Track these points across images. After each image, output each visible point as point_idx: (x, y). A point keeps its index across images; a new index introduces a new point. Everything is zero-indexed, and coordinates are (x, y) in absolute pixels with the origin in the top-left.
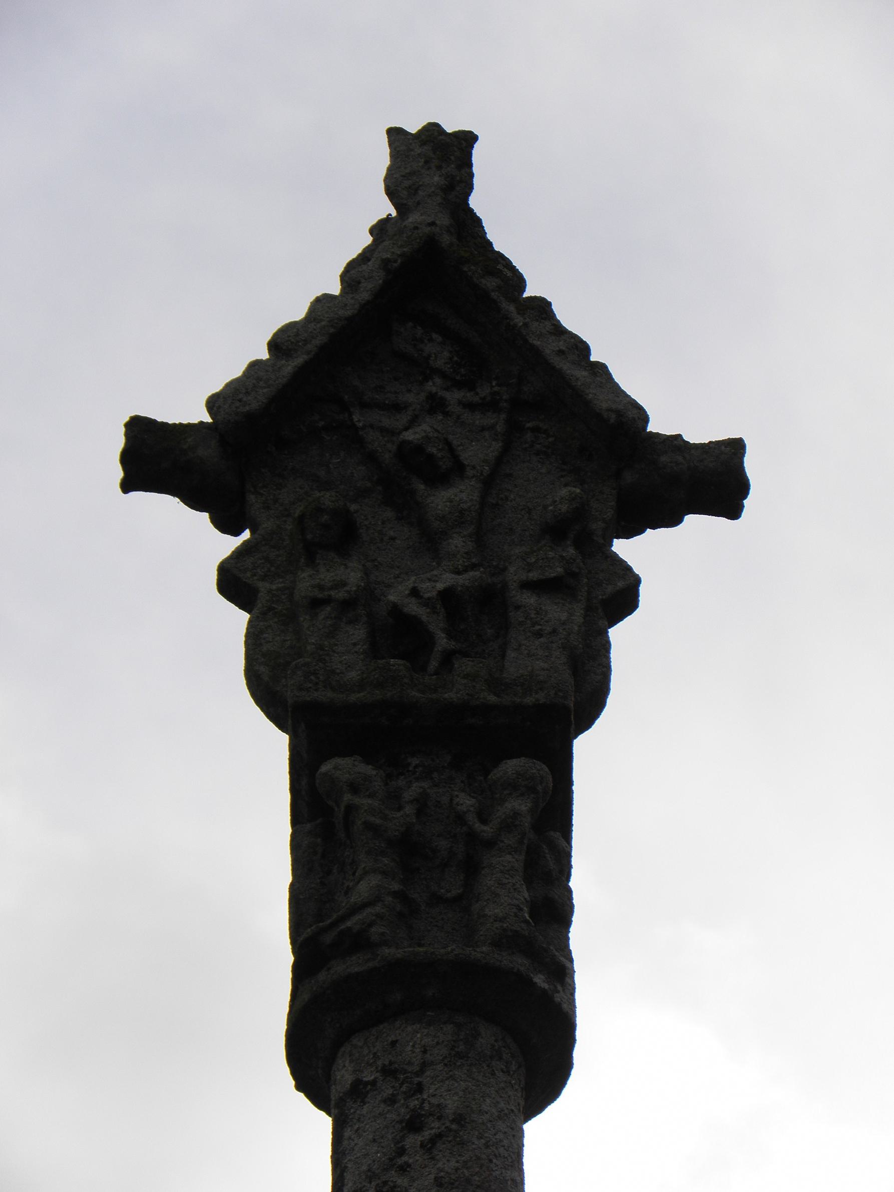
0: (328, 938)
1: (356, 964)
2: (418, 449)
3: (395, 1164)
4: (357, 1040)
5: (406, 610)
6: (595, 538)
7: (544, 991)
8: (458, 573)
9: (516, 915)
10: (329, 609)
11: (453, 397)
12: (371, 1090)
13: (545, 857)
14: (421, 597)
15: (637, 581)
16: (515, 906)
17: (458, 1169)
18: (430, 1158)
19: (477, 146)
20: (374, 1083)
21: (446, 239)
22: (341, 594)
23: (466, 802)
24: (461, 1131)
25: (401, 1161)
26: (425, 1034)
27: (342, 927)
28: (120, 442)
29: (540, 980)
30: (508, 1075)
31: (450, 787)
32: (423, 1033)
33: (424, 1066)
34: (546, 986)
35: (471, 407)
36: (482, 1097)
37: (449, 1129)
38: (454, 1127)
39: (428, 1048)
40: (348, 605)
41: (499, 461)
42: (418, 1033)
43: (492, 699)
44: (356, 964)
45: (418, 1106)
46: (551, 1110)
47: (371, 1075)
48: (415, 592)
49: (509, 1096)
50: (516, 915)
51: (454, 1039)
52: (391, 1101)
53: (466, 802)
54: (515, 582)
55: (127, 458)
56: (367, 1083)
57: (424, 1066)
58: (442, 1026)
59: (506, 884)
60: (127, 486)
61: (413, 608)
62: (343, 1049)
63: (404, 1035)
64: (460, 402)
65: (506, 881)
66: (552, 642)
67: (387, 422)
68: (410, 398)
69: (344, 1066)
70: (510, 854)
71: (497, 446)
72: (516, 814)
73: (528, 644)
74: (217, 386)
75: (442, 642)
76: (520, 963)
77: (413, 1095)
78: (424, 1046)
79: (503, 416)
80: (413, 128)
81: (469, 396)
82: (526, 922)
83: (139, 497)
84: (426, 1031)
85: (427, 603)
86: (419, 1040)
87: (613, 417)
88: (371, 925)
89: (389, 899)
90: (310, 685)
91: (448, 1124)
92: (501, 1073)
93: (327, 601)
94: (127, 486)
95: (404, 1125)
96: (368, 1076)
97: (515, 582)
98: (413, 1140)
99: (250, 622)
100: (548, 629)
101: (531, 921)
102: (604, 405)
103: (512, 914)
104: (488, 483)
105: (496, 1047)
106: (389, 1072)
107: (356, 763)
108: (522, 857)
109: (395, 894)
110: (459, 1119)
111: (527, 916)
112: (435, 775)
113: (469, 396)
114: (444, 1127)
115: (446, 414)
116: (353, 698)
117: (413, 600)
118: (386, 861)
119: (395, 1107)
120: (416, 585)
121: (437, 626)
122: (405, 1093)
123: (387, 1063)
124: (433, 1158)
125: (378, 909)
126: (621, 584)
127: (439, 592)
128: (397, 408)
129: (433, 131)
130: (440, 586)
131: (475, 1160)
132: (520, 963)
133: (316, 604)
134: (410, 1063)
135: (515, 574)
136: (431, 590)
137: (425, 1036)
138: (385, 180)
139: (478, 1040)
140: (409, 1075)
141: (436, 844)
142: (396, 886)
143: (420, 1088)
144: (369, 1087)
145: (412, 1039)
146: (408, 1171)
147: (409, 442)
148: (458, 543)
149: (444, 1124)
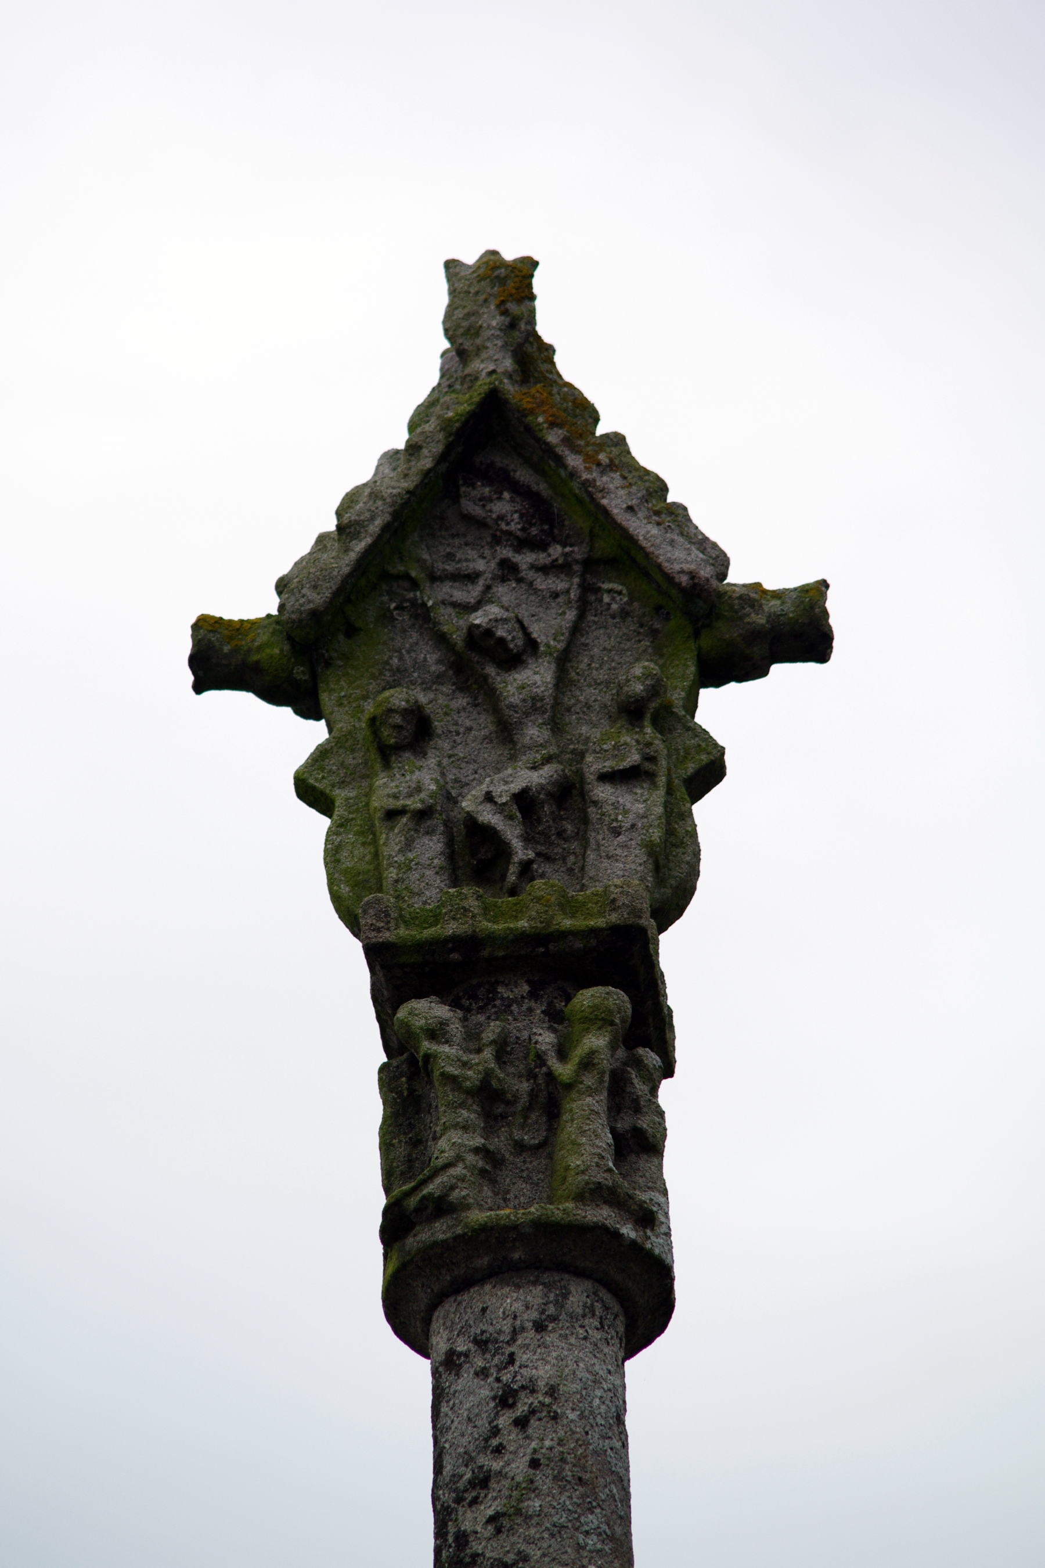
0: (413, 1202)
1: (440, 1231)
2: (488, 633)
3: (490, 1446)
4: (449, 1305)
5: (481, 819)
6: (675, 710)
7: (633, 1242)
8: (534, 768)
9: (598, 1165)
10: (405, 820)
11: (525, 559)
12: (464, 1362)
13: (632, 1083)
14: (496, 803)
15: (722, 751)
16: (598, 1155)
17: (554, 1447)
18: (524, 1438)
19: (538, 274)
20: (466, 1355)
21: (510, 388)
22: (415, 804)
23: (546, 1039)
24: (554, 1404)
25: (495, 1442)
26: (514, 1298)
27: (425, 1192)
28: (186, 646)
29: (628, 1231)
30: (603, 1331)
31: (529, 1020)
32: (512, 1297)
33: (515, 1333)
34: (633, 1235)
35: (544, 570)
36: (576, 1362)
37: (542, 1404)
38: (547, 1400)
39: (518, 1314)
40: (423, 815)
41: (576, 629)
42: (507, 1297)
43: (567, 923)
44: (440, 1231)
45: (510, 1380)
46: (660, 1343)
47: (464, 1346)
48: (489, 798)
49: (605, 1355)
50: (598, 1165)
51: (544, 1301)
52: (482, 1373)
53: (546, 1039)
54: (591, 774)
55: (196, 662)
56: (460, 1354)
57: (515, 1333)
58: (531, 1288)
59: (587, 1130)
60: (199, 688)
61: (488, 816)
62: (436, 1314)
63: (494, 1300)
64: (533, 567)
65: (587, 1128)
66: (631, 839)
67: (460, 595)
68: (480, 565)
69: (439, 1333)
70: (590, 1096)
71: (571, 615)
72: (592, 1053)
73: (606, 845)
74: (285, 568)
75: (521, 852)
76: (603, 1214)
77: (505, 1368)
78: (514, 1312)
79: (576, 580)
80: (470, 257)
81: (542, 558)
82: (610, 1170)
83: (214, 697)
84: (515, 1295)
85: (501, 808)
86: (509, 1305)
87: (684, 579)
88: (452, 1188)
89: (471, 1158)
90: (382, 924)
91: (541, 1398)
92: (596, 1331)
93: (401, 812)
94: (199, 688)
95: (497, 1401)
96: (462, 1346)
97: (591, 774)
98: (504, 1420)
99: (330, 833)
100: (626, 825)
101: (614, 1169)
102: (677, 567)
103: (594, 1164)
104: (564, 660)
105: (588, 1305)
106: (482, 1343)
107: (433, 1005)
108: (604, 1095)
109: (476, 1150)
110: (552, 1391)
111: (611, 1164)
112: (514, 1007)
113: (542, 558)
114: (537, 1402)
115: (520, 580)
116: (429, 933)
117: (489, 806)
118: (465, 1113)
119: (488, 1381)
120: (491, 789)
121: (512, 833)
122: (496, 1365)
123: (478, 1332)
124: (527, 1437)
125: (459, 1170)
126: (704, 758)
127: (514, 795)
128: (472, 577)
129: (491, 260)
130: (516, 787)
131: (570, 1435)
132: (603, 1214)
133: (392, 815)
134: (500, 1332)
135: (594, 765)
136: (503, 792)
137: (515, 1300)
138: (444, 322)
139: (568, 1299)
140: (501, 1345)
141: (517, 1087)
142: (478, 1141)
143: (511, 1359)
144: (463, 1358)
145: (502, 1305)
146: (504, 1454)
147: (478, 626)
148: (533, 732)
149: (537, 1398)
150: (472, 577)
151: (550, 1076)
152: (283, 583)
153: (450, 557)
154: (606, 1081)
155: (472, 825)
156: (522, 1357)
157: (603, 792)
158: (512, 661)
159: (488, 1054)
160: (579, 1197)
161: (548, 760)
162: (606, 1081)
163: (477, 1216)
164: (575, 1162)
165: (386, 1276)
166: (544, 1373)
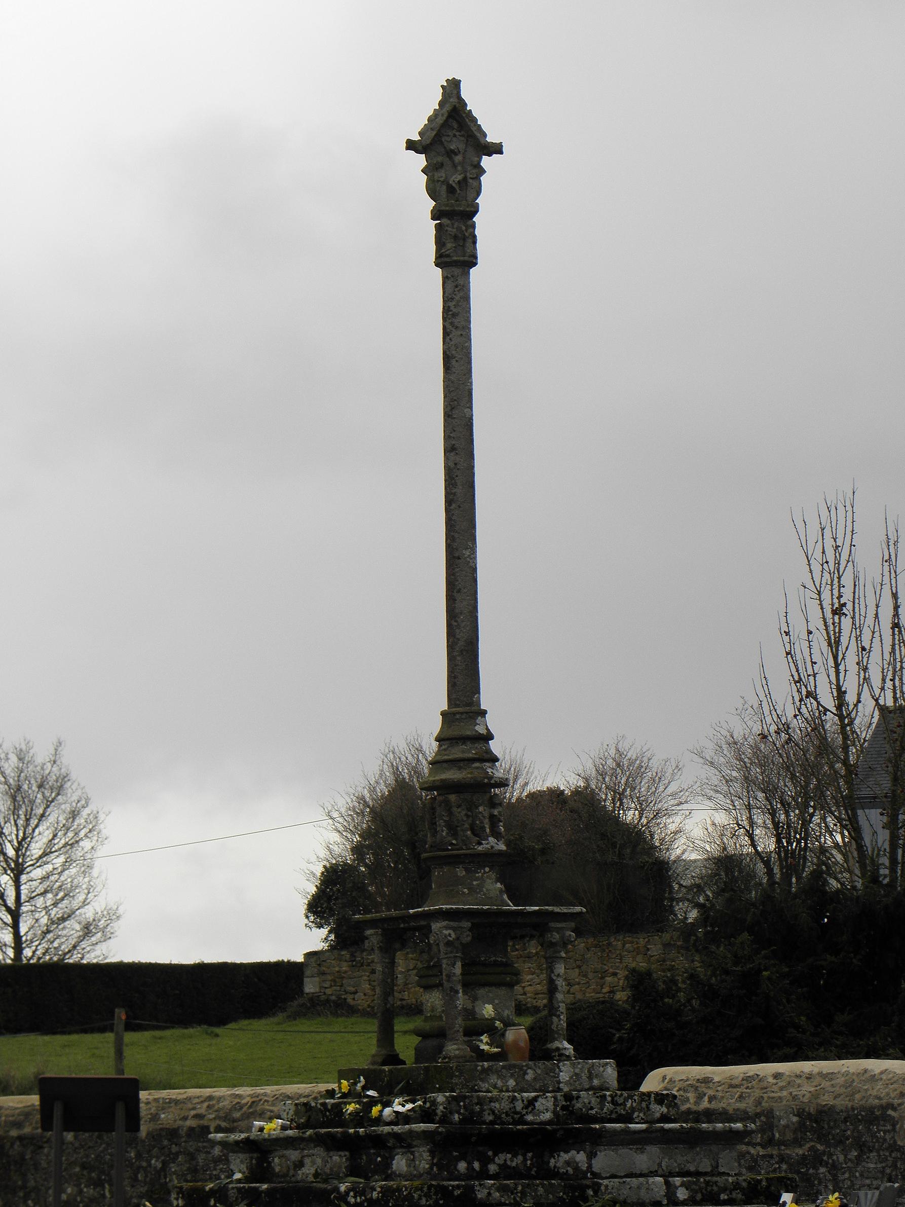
23: (464, 228)
61: (454, 185)
85: (456, 183)
106: (452, 276)
148: (459, 168)
150: (448, 136)
151: (464, 234)
152: (707, 1080)
153: (446, 132)
154: (777, 873)
155: (452, 186)
156: (459, 280)
157: (471, 181)
158: (456, 154)
159: (455, 230)
160: (469, 257)
161: (462, 173)
162: (777, 873)
163: (455, 258)
164: (468, 251)
165: (446, 295)
166: (462, 283)
